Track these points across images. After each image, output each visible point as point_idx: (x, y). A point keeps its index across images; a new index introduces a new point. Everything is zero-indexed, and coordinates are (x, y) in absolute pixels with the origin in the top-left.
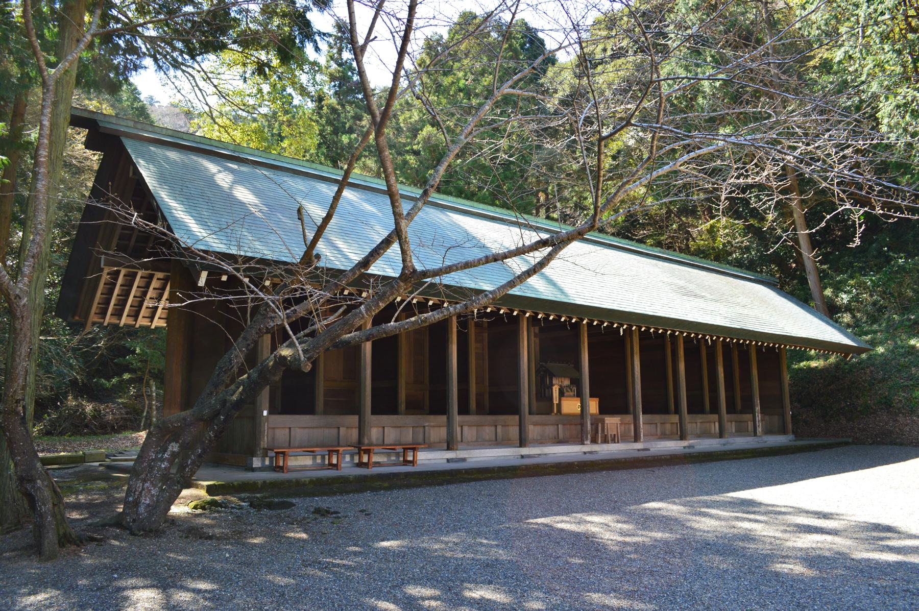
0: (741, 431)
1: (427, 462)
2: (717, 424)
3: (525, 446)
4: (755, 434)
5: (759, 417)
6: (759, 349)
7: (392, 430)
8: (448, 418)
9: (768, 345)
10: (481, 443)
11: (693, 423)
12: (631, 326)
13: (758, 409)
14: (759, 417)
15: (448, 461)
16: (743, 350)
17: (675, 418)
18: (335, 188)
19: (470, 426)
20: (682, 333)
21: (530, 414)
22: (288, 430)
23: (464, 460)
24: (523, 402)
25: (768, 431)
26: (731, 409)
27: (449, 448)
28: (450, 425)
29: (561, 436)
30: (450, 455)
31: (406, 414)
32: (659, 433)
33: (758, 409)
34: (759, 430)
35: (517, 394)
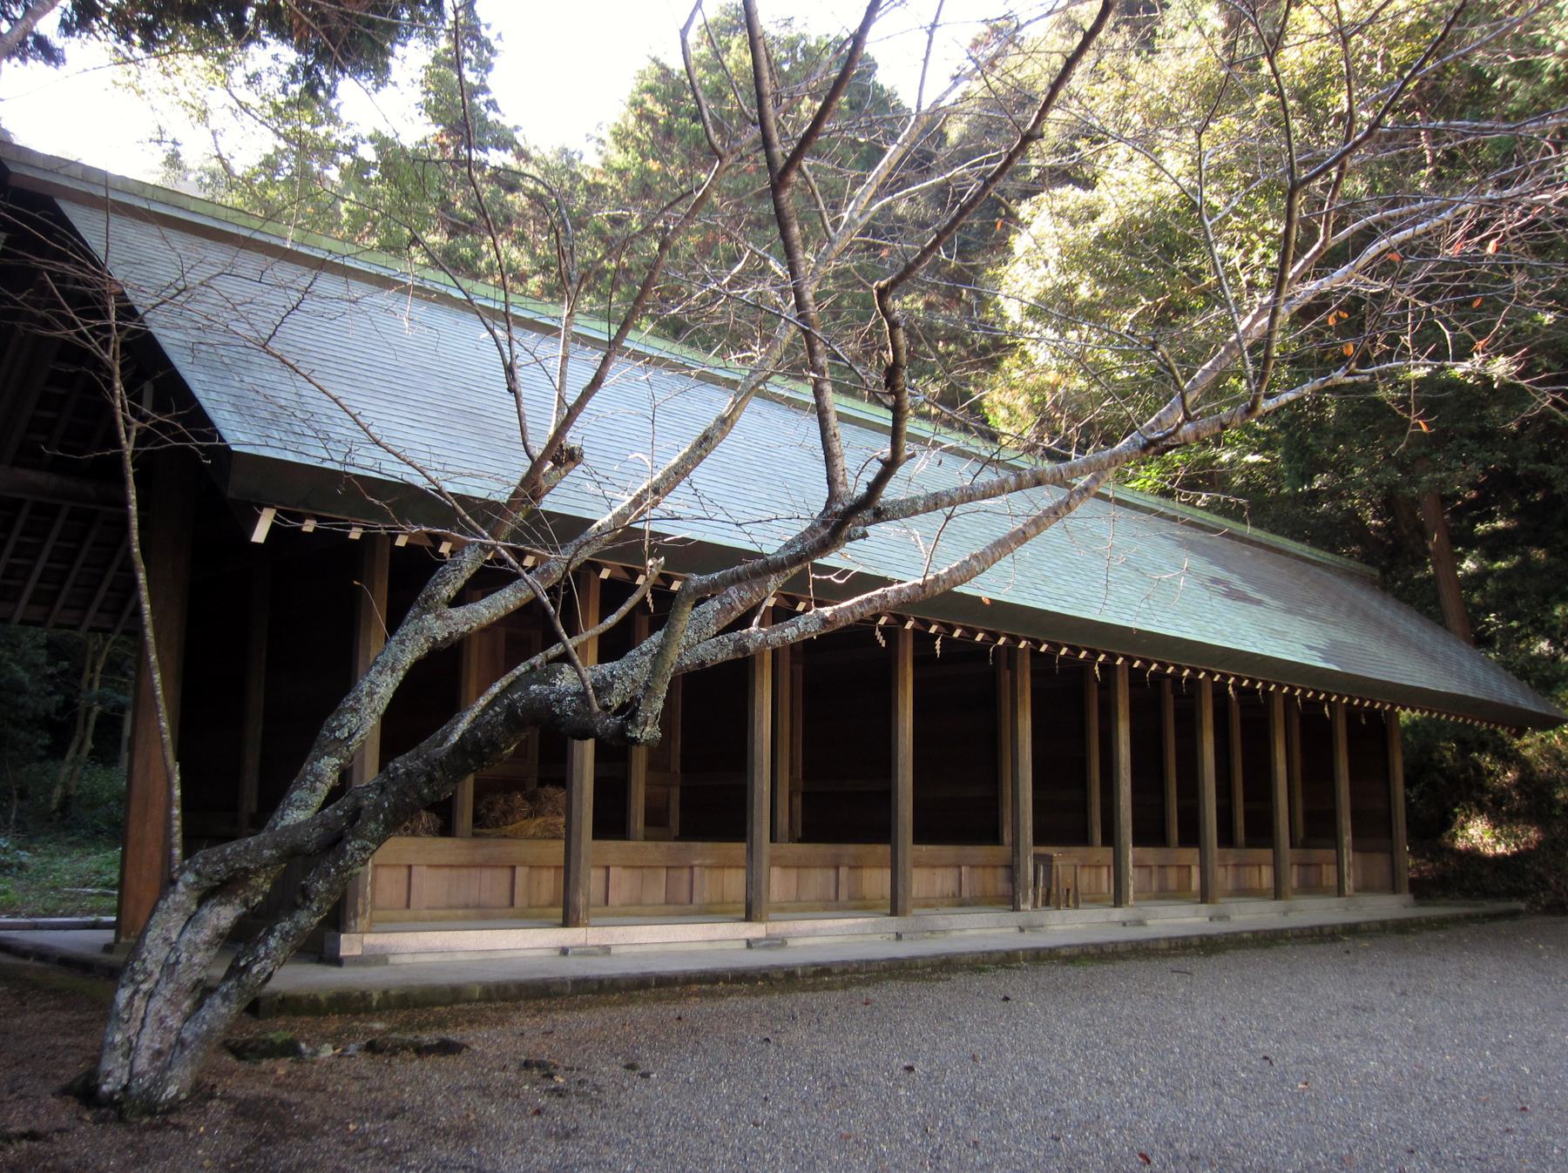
0: (1310, 888)
1: (705, 946)
2: (1195, 872)
3: (576, 924)
4: (1340, 892)
5: (1348, 856)
6: (1352, 714)
7: (626, 873)
8: (750, 851)
9: (1350, 704)
10: (637, 912)
11: (931, 872)
12: (1112, 657)
13: (1347, 838)
14: (1348, 856)
15: (749, 944)
16: (1188, 695)
17: (1191, 855)
18: (599, 356)
19: (972, 867)
20: (1211, 674)
21: (1292, 846)
22: (405, 872)
23: (606, 950)
24: (900, 813)
25: (1365, 888)
26: (1226, 839)
27: (749, 918)
28: (750, 864)
29: (966, 894)
30: (756, 930)
31: (646, 839)
32: (1155, 886)
33: (1347, 838)
34: (1349, 884)
35: (886, 797)
